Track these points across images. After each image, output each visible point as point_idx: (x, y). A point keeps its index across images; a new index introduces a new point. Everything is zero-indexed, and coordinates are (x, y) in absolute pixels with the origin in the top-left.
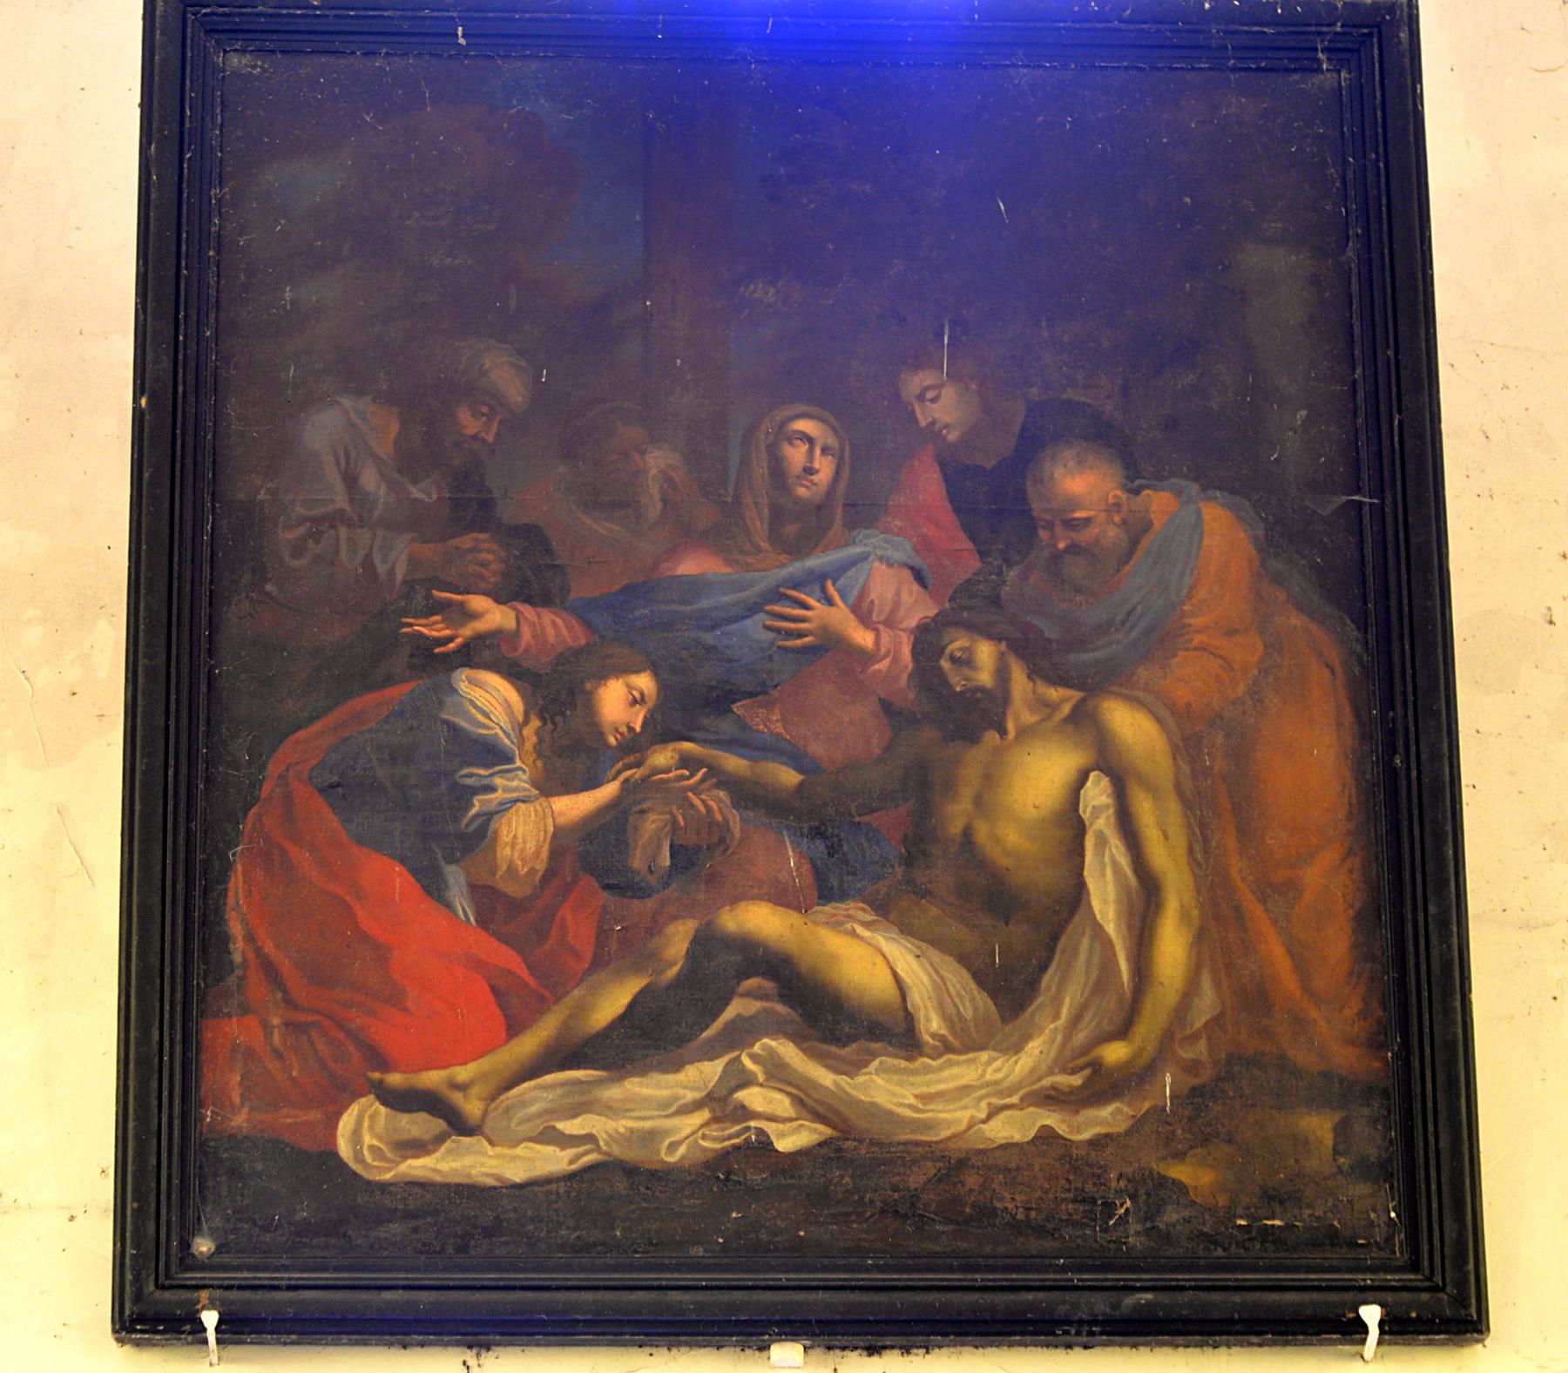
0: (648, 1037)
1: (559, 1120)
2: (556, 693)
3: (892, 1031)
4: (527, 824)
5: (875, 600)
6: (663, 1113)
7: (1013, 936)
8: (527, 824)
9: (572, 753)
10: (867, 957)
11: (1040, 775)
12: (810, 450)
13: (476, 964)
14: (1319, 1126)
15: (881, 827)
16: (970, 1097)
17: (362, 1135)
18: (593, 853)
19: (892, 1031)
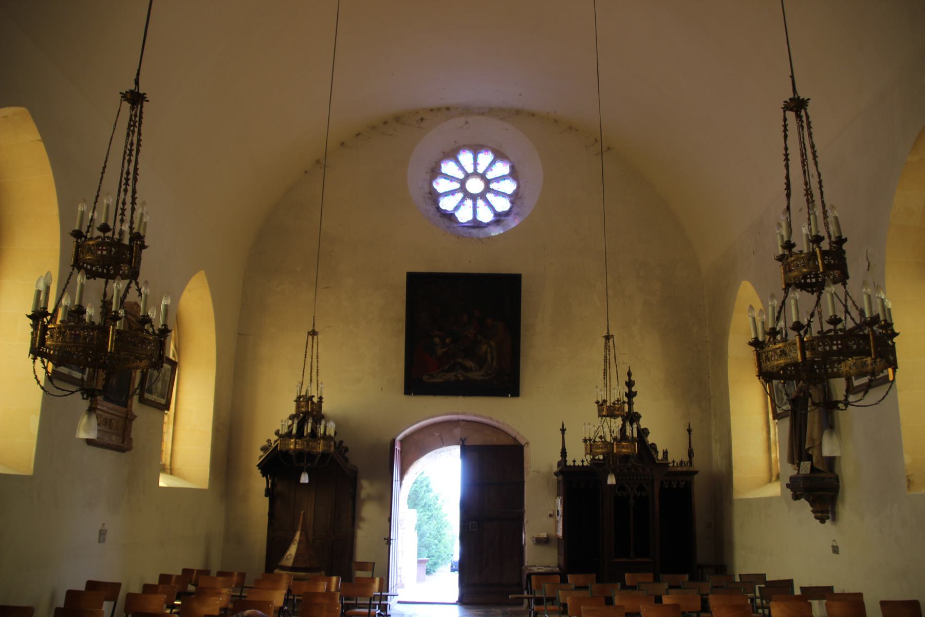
4: (440, 351)
6: (451, 376)
8: (440, 351)
10: (469, 364)
11: (484, 347)
16: (477, 375)
17: (425, 378)
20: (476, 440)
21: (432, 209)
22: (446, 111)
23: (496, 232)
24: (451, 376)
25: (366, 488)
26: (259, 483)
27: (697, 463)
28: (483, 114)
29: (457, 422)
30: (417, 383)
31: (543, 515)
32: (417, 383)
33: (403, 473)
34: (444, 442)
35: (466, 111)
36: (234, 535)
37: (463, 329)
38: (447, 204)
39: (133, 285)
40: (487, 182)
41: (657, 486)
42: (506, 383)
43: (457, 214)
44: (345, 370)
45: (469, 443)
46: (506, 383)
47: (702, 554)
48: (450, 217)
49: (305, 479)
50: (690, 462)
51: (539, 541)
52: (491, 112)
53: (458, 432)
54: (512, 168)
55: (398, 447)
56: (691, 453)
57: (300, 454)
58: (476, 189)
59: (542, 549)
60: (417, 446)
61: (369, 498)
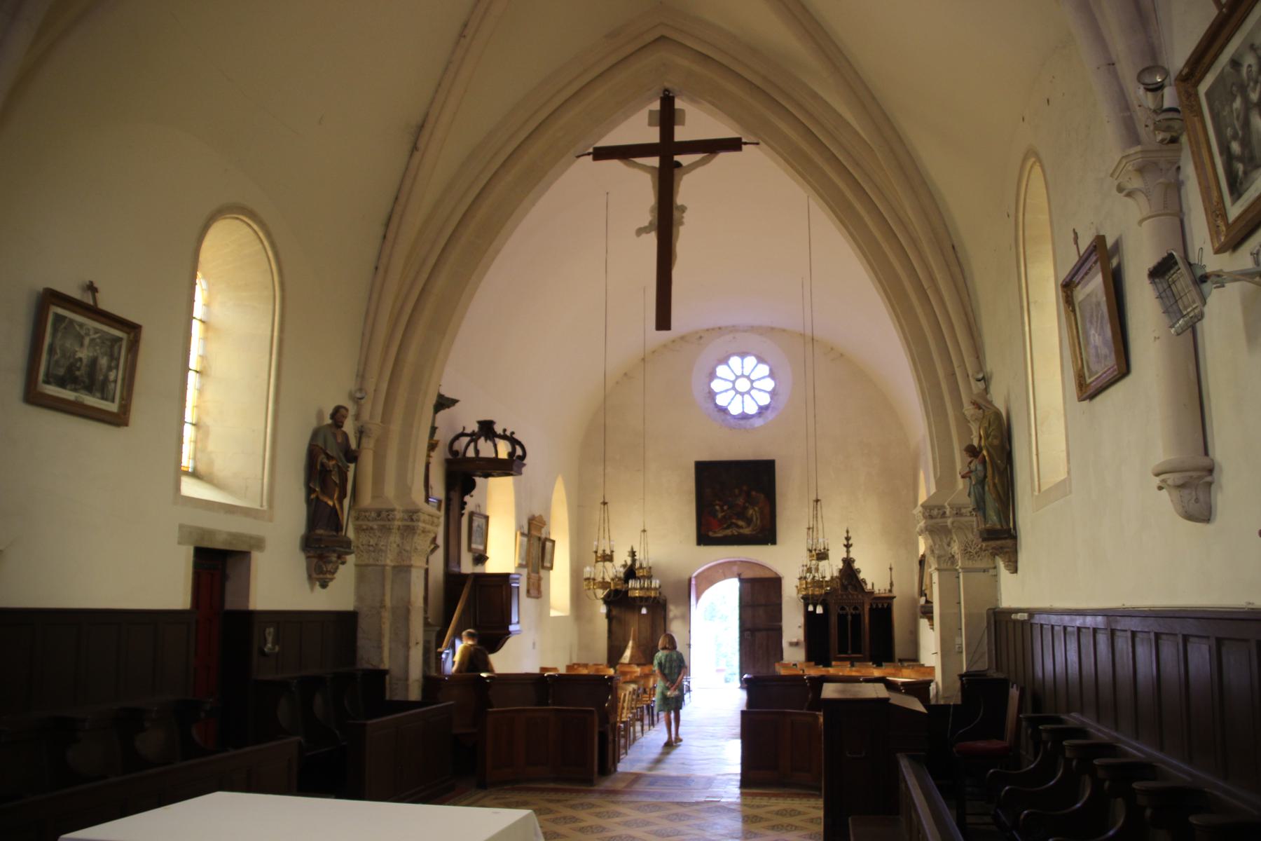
0: (728, 528)
1: (601, 137)
2: (722, 507)
3: (741, 527)
4: (720, 515)
5: (740, 501)
6: (728, 532)
7: (749, 521)
8: (720, 515)
9: (723, 510)
10: (741, 523)
11: (751, 512)
12: (737, 491)
13: (582, 821)
14: (225, 404)
15: (742, 515)
16: (747, 531)
17: (711, 534)
18: (724, 517)
19: (741, 527)
20: (749, 574)
21: (712, 406)
22: (719, 330)
23: (758, 423)
24: (728, 532)
25: (673, 611)
26: (603, 609)
27: (895, 592)
28: (745, 331)
29: (734, 563)
30: (704, 538)
31: (793, 627)
32: (704, 538)
33: (698, 599)
34: (725, 576)
35: (734, 329)
36: (584, 644)
37: (735, 498)
38: (721, 400)
39: (472, 445)
40: (752, 382)
41: (867, 608)
42: (767, 535)
43: (730, 408)
44: (655, 532)
45: (743, 576)
46: (767, 535)
47: (899, 649)
48: (724, 410)
49: (644, 611)
50: (890, 591)
51: (792, 644)
52: (752, 329)
53: (735, 569)
54: (771, 370)
55: (693, 582)
56: (891, 585)
57: (641, 598)
58: (743, 386)
59: (794, 649)
60: (709, 578)
61: (675, 617)
